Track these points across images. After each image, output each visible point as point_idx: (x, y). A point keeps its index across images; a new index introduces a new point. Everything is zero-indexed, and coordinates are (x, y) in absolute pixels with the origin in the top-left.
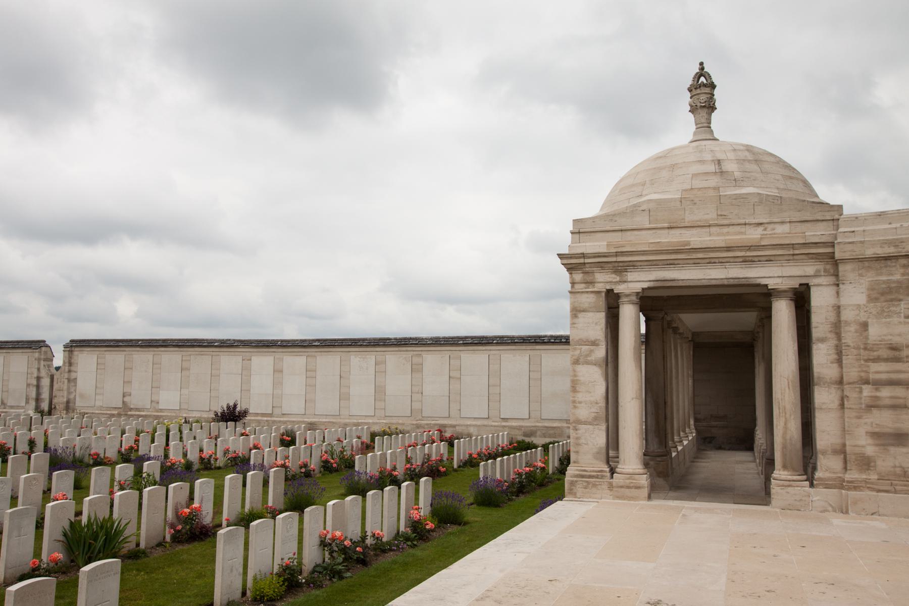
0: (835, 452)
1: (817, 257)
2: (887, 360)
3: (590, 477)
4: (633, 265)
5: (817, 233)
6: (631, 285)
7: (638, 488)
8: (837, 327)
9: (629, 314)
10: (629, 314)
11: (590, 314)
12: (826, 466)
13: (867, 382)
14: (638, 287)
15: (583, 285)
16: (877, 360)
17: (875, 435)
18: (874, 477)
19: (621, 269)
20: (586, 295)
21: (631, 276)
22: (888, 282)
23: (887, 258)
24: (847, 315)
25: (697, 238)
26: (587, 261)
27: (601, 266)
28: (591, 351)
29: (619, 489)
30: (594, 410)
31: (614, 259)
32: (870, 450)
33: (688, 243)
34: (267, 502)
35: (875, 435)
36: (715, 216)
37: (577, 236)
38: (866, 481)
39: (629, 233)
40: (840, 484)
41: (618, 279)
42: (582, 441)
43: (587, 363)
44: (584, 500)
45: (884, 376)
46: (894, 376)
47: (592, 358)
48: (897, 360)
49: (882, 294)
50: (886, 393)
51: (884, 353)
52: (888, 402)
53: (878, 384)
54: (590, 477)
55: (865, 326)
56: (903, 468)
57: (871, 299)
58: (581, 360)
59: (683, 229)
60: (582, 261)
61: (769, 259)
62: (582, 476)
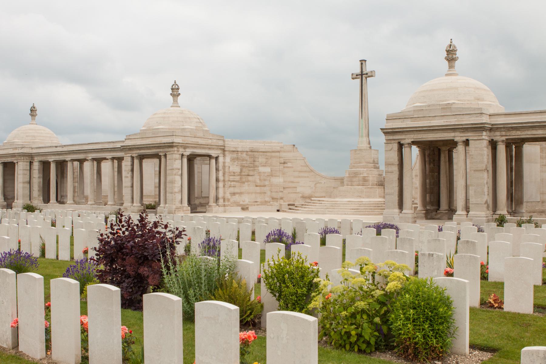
0: (222, 198)
1: (221, 149)
2: (233, 176)
3: (179, 208)
4: (188, 147)
5: (221, 143)
6: (187, 153)
7: (189, 210)
8: (224, 166)
9: (502, 149)
10: (502, 149)
11: (178, 160)
12: (221, 201)
13: (229, 181)
14: (188, 153)
15: (176, 152)
16: (231, 175)
17: (230, 193)
18: (230, 203)
19: (185, 147)
20: (177, 155)
21: (187, 150)
22: (234, 157)
23: (234, 151)
24: (227, 164)
25: (201, 141)
26: (180, 145)
27: (181, 146)
28: (178, 172)
29: (186, 211)
30: (179, 189)
31: (185, 145)
32: (229, 197)
33: (198, 142)
34: (510, 149)
35: (230, 193)
36: (202, 135)
37: (386, 144)
38: (229, 204)
39: (186, 137)
40: (224, 206)
41: (184, 151)
42: (176, 198)
43: (177, 175)
44: (427, 166)
45: (232, 180)
46: (234, 179)
47: (178, 174)
48: (234, 176)
49: (233, 160)
50: (232, 183)
51: (232, 174)
52: (233, 185)
53: (231, 181)
54: (179, 208)
55: (229, 167)
56: (217, 205)
57: (231, 161)
58: (176, 174)
59: (169, 137)
60: (178, 144)
61: (213, 149)
62: (177, 208)
